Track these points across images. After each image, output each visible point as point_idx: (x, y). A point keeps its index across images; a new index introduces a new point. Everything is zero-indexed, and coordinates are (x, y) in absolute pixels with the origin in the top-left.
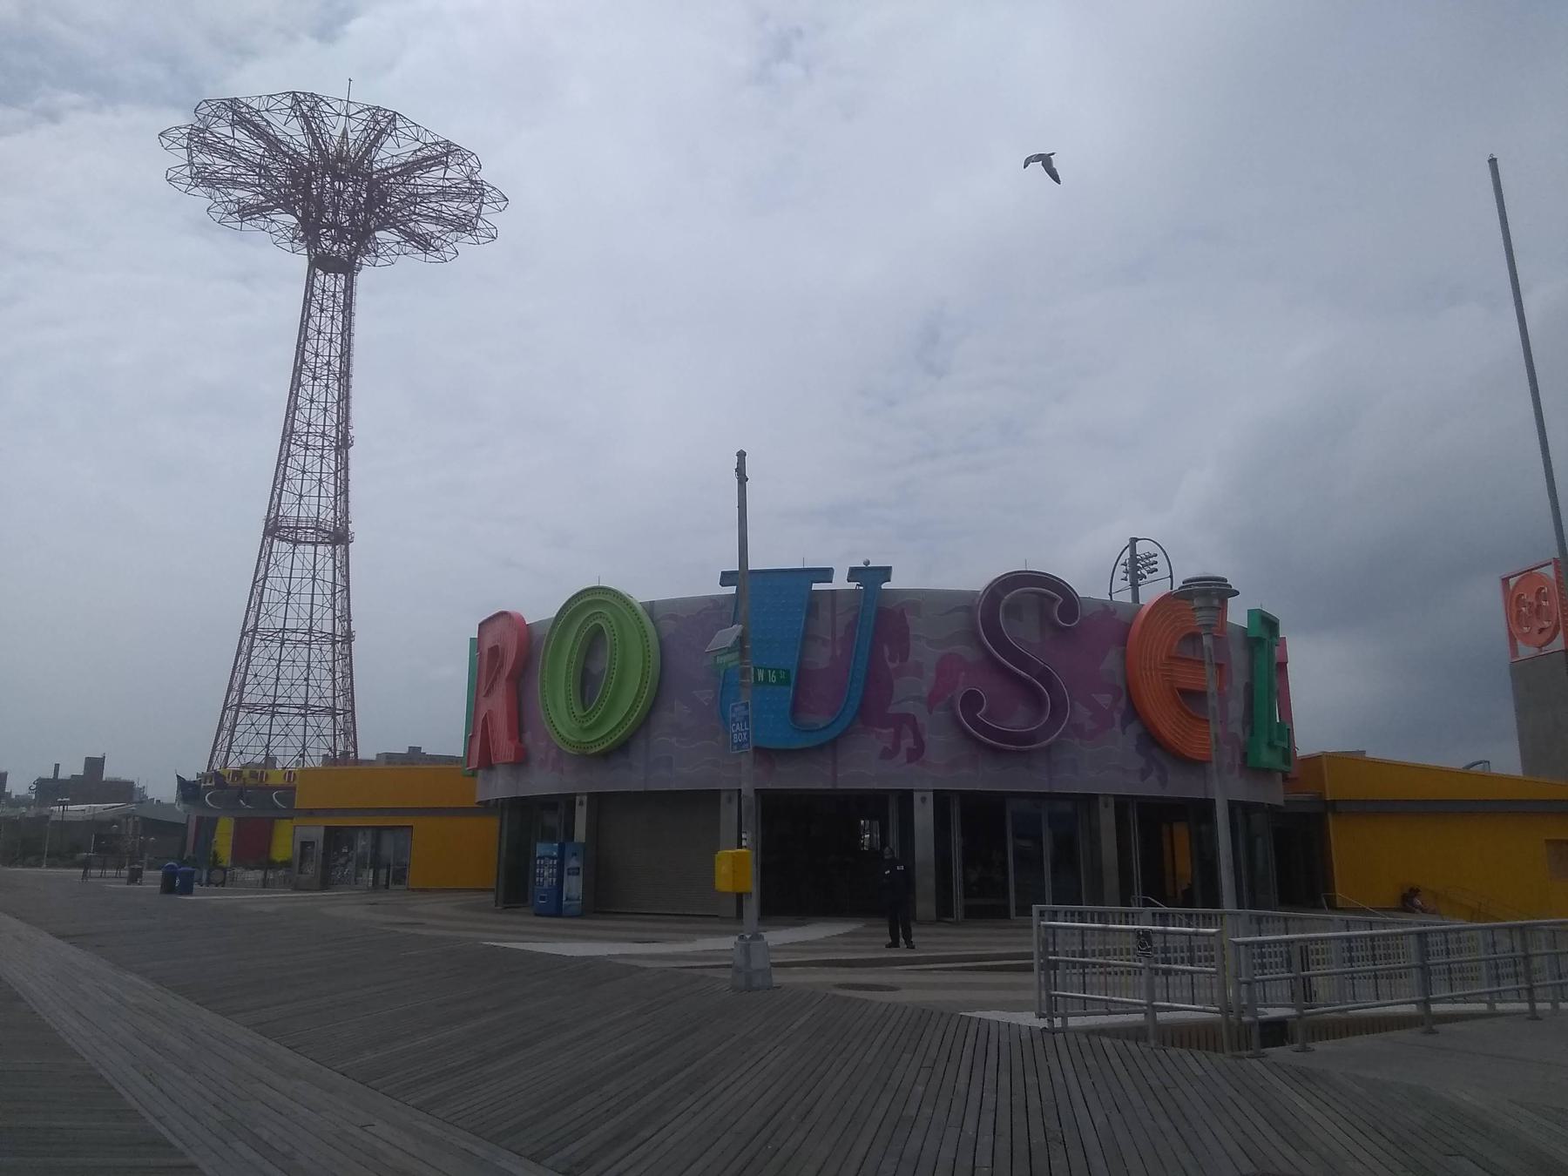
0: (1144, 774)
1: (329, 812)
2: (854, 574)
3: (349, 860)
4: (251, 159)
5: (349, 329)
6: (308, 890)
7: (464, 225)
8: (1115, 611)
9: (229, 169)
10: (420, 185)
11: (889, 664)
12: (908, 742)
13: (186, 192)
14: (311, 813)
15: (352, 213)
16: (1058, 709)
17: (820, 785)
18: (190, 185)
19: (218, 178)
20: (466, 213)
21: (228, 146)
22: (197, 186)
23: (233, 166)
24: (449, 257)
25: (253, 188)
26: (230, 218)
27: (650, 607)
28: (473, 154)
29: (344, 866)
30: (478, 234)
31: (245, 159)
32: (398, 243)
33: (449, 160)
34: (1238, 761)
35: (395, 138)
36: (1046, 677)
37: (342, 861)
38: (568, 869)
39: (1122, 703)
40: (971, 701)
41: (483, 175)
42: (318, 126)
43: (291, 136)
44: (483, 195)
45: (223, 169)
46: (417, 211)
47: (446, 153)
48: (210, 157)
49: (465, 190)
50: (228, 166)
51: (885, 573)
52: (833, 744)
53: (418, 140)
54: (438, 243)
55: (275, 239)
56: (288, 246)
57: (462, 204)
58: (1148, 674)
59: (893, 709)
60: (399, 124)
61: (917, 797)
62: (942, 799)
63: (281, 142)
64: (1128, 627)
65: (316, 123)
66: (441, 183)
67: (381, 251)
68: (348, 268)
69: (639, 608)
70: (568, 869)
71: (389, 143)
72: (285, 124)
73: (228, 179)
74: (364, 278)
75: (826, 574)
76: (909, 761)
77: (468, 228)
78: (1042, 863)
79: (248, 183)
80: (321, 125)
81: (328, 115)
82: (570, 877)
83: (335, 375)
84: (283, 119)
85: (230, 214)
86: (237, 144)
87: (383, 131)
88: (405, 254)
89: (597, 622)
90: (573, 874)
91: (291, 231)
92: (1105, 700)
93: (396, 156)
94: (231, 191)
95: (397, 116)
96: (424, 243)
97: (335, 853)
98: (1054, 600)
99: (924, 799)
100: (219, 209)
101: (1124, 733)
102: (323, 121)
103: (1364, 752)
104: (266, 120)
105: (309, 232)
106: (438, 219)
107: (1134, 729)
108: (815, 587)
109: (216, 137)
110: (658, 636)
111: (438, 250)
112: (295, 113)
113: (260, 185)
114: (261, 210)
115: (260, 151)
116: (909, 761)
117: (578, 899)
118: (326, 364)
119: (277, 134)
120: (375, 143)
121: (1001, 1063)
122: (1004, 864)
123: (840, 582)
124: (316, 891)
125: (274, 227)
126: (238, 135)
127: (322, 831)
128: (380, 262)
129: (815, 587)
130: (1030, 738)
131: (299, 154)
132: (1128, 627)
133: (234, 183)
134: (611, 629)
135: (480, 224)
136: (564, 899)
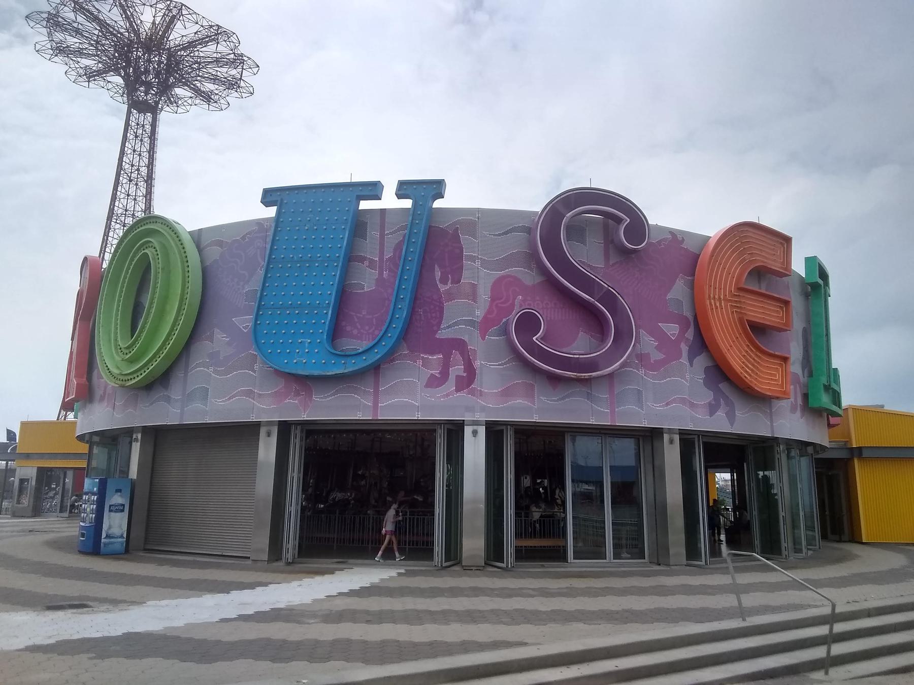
0: (712, 409)
1: (42, 456)
2: (404, 189)
3: (56, 494)
4: (90, 37)
5: (154, 149)
6: (23, 517)
7: (233, 84)
8: (683, 240)
9: (77, 45)
10: (202, 57)
11: (440, 286)
12: (457, 369)
13: (49, 60)
14: (28, 456)
15: (157, 74)
16: (623, 337)
17: (359, 416)
18: (52, 55)
19: (70, 51)
20: (233, 77)
21: (75, 28)
22: (56, 56)
23: (79, 43)
24: (224, 107)
25: (93, 58)
26: (81, 79)
27: (197, 236)
28: (234, 33)
29: (53, 498)
30: (241, 91)
31: (86, 37)
32: (191, 97)
33: (219, 38)
34: (800, 401)
35: (182, 22)
36: (610, 300)
37: (51, 494)
38: (110, 506)
39: (690, 334)
40: (528, 323)
41: (241, 50)
42: (132, 14)
43: (115, 22)
44: (243, 63)
45: (73, 45)
46: (201, 74)
47: (216, 34)
48: (63, 35)
49: (231, 60)
50: (77, 43)
51: (436, 188)
52: (375, 369)
53: (197, 23)
54: (217, 97)
55: (112, 94)
56: (120, 99)
57: (230, 69)
58: (718, 304)
59: (444, 334)
60: (184, 12)
61: (468, 430)
62: (494, 432)
63: (108, 25)
64: (696, 257)
65: (130, 12)
66: (215, 55)
67: (180, 102)
68: (154, 110)
69: (187, 239)
70: (110, 506)
71: (179, 25)
72: (110, 11)
73: (77, 51)
74: (166, 116)
75: (373, 190)
76: (458, 390)
77: (235, 87)
78: (602, 501)
79: (90, 54)
80: (135, 13)
81: (137, 4)
82: (112, 514)
83: (143, 178)
84: (108, 7)
85: (80, 76)
86: (80, 27)
87: (174, 17)
88: (195, 105)
89: (145, 251)
90: (117, 511)
91: (122, 89)
92: (672, 329)
93: (185, 36)
94: (79, 59)
95: (183, 7)
96: (207, 98)
97: (47, 488)
98: (619, 221)
99: (475, 433)
100: (73, 73)
101: (691, 365)
102: (135, 10)
103: (882, 406)
104: (97, 9)
105: (131, 87)
106: (215, 79)
107: (702, 362)
108: (364, 205)
109: (66, 21)
110: (202, 262)
111: (216, 102)
112: (116, 4)
113: (98, 55)
114: (100, 73)
115: (96, 32)
116: (458, 390)
117: (122, 537)
118: (136, 170)
119: (106, 19)
120: (169, 25)
121: (618, 291)
122: (564, 503)
123: (389, 201)
124: (28, 517)
125: (110, 86)
126: (80, 19)
127: (35, 471)
128: (180, 110)
129: (364, 205)
130: (591, 365)
131: (121, 34)
132: (695, 258)
133: (80, 53)
134: (157, 257)
135: (242, 84)
136: (104, 535)
